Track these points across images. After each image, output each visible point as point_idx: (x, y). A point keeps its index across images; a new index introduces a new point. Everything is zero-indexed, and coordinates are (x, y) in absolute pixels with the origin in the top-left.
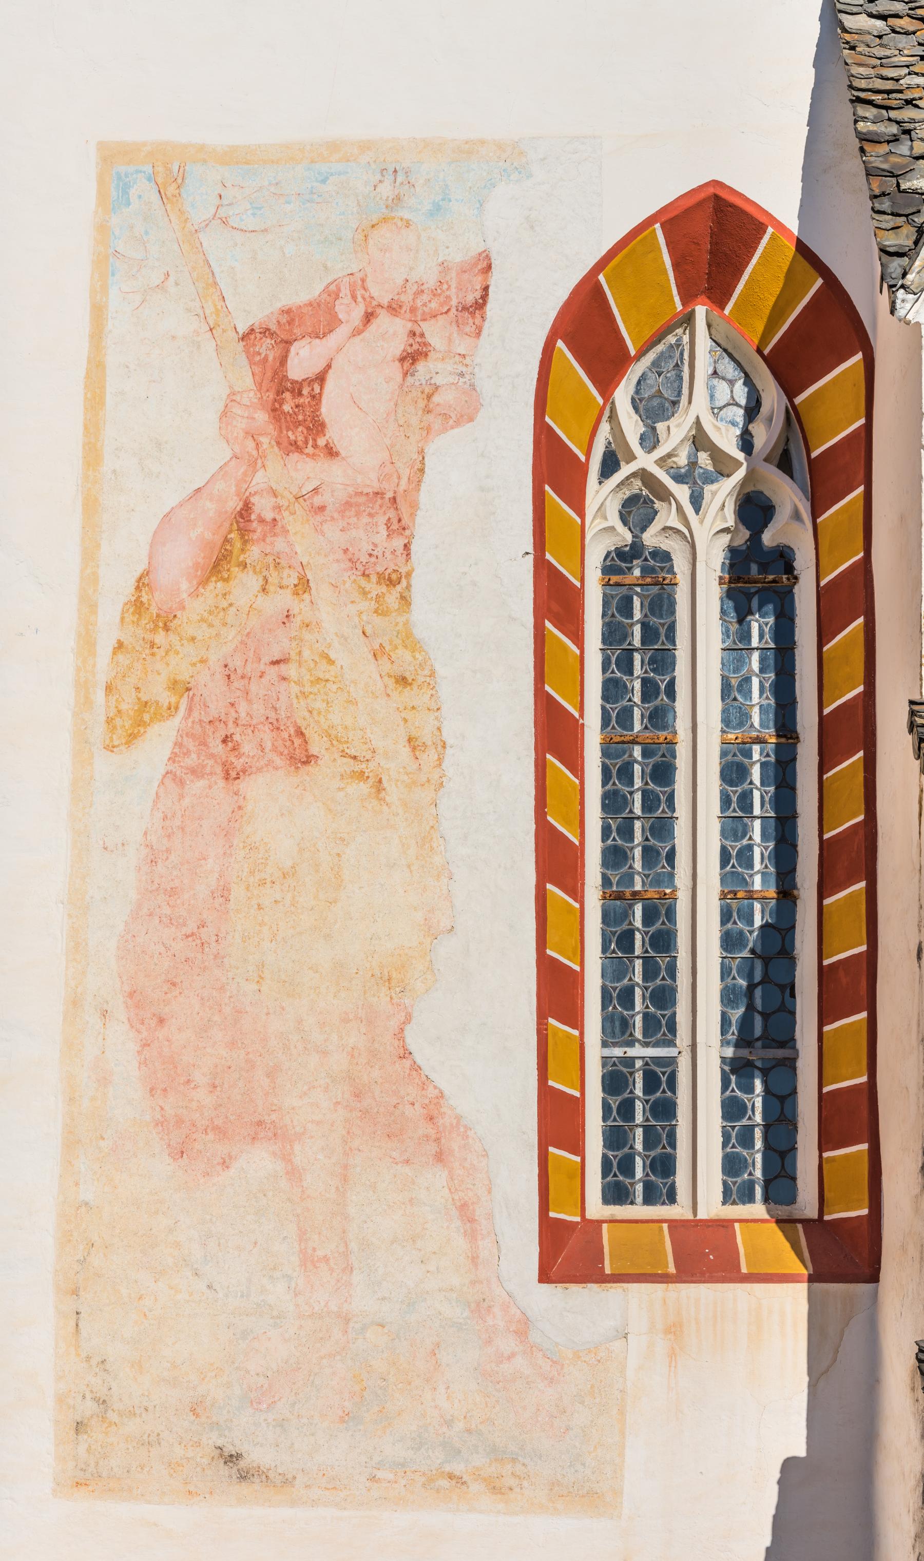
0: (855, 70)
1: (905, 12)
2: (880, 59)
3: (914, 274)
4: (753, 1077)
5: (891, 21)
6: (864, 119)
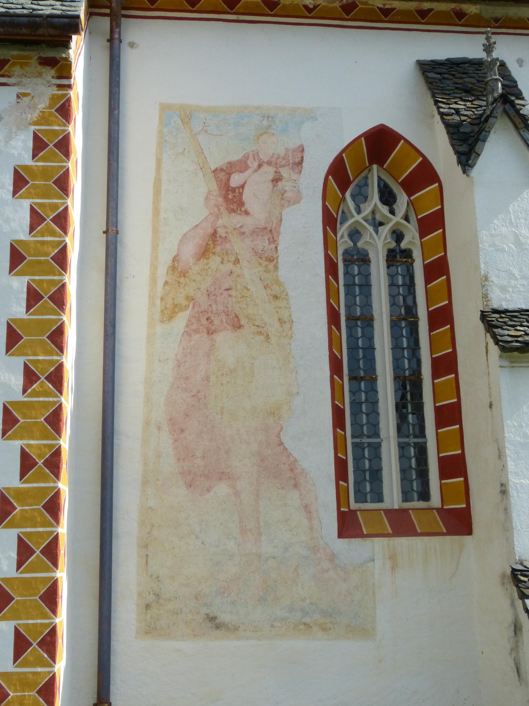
6: (442, 108)
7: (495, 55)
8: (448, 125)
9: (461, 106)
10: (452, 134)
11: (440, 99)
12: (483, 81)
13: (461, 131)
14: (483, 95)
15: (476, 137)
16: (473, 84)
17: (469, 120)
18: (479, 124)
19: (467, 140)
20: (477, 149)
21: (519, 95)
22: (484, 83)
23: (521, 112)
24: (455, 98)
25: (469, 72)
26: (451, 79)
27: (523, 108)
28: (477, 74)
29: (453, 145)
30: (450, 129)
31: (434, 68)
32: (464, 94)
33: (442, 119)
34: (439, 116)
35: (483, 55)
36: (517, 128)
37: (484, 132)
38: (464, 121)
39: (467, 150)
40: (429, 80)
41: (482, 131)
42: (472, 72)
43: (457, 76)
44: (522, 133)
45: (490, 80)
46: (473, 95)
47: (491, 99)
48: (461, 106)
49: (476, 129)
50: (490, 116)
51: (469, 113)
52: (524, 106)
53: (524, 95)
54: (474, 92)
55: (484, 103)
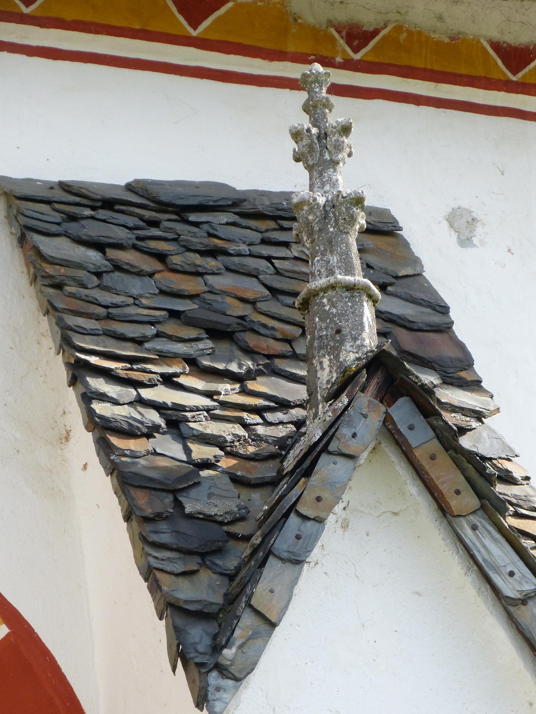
0: (72, 321)
1: (130, 242)
2: (106, 307)
3: (234, 650)
4: (398, 354)
5: (112, 253)
6: (103, 397)
7: (347, 179)
8: (127, 481)
9: (190, 396)
10: (146, 519)
11: (94, 360)
12: (295, 294)
13: (188, 509)
14: (295, 357)
15: (256, 540)
16: (253, 303)
17: (226, 463)
18: (273, 483)
19: (219, 551)
20: (261, 594)
21: (459, 371)
22: (297, 302)
23: (465, 442)
24: (164, 357)
25: (232, 248)
26: (151, 275)
27: (474, 424)
28: (269, 259)
29: (149, 574)
30: (142, 499)
31: (73, 218)
32: (208, 344)
33: (104, 448)
34: (89, 436)
35: (288, 179)
36: (443, 509)
37: (293, 519)
38: (206, 465)
39: (217, 598)
40: (50, 269)
41: (286, 515)
42: (244, 248)
43: (176, 260)
44: (468, 534)
45: (325, 290)
46: (249, 352)
47: (326, 375)
48: (190, 396)
49: (259, 502)
50: (325, 449)
51: (228, 431)
52: (479, 416)
53: (481, 368)
54: (251, 340)
55: (299, 392)
